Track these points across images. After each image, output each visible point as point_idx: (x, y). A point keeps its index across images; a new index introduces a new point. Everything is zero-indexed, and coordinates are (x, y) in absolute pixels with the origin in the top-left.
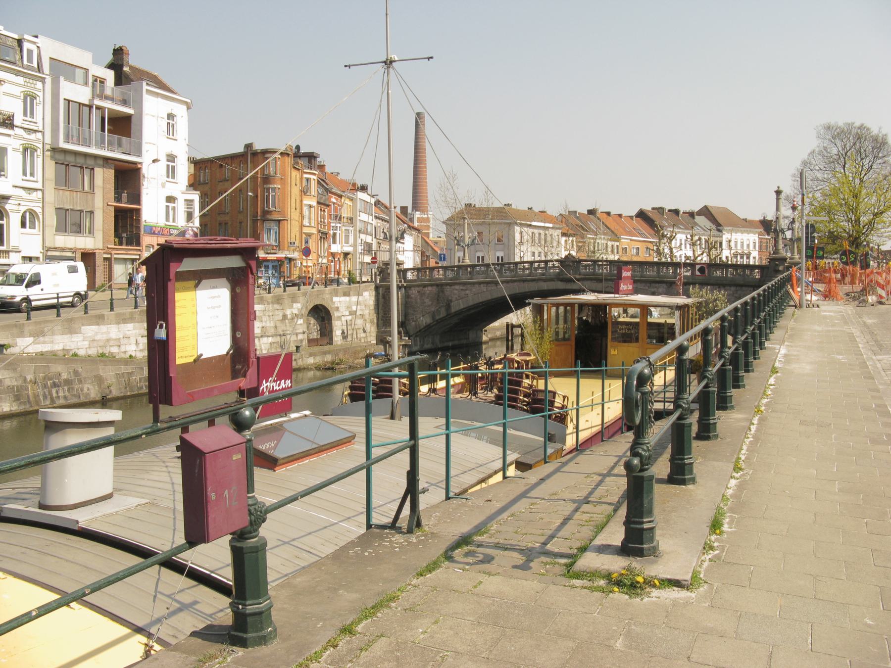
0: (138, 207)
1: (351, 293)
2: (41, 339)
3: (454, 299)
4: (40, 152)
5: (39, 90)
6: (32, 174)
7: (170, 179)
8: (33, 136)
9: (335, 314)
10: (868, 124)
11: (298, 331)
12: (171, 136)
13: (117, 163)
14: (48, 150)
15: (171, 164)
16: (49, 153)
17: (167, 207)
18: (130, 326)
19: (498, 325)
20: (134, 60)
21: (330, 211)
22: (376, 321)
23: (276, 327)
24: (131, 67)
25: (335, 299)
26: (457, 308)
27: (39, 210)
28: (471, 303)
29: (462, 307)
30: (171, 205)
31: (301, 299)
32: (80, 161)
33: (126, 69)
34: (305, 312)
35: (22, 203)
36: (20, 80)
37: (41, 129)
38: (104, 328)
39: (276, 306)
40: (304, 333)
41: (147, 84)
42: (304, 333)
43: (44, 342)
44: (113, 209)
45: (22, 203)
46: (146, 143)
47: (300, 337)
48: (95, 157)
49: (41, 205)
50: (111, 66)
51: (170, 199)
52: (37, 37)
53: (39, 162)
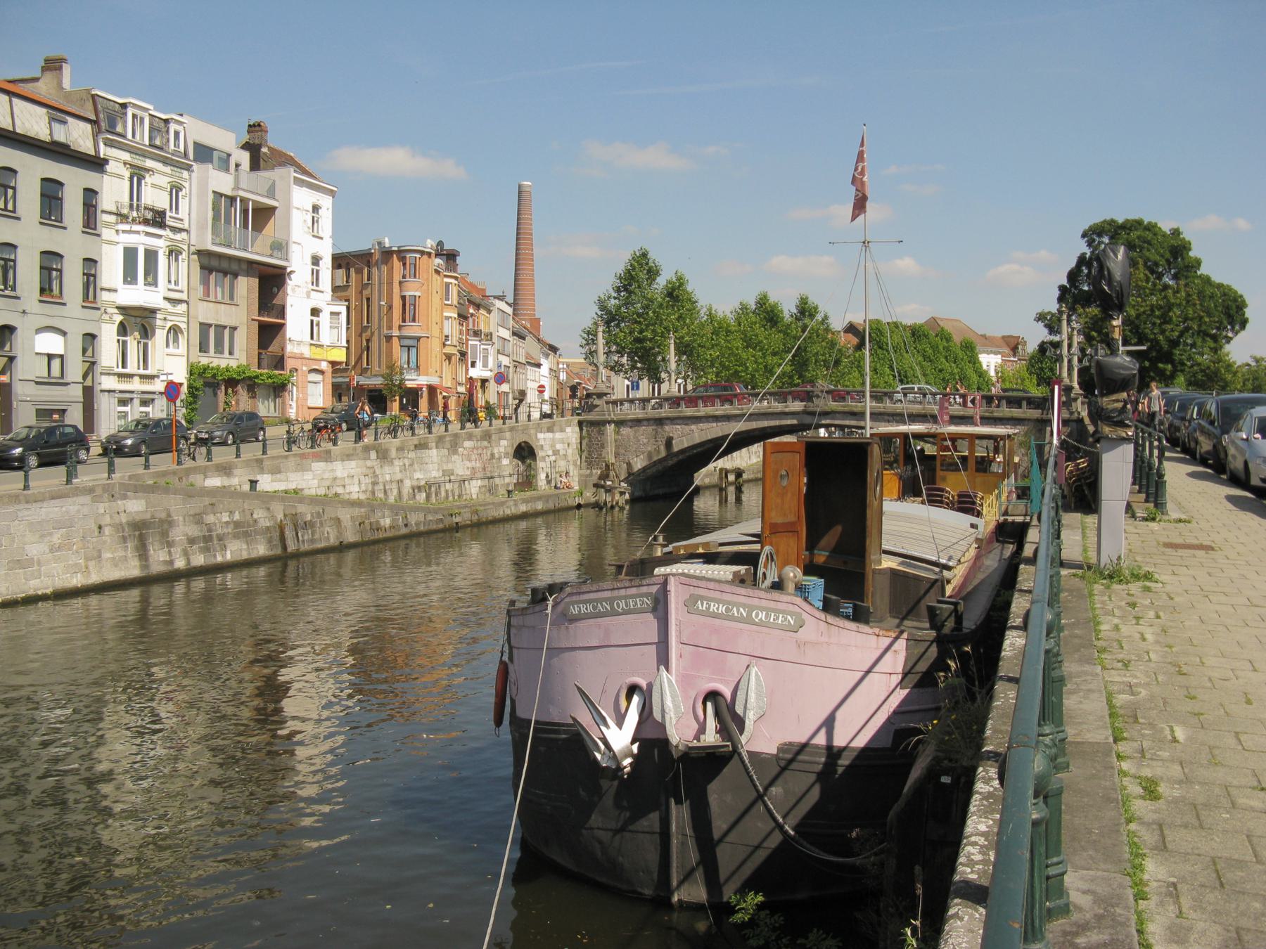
0: (282, 321)
1: (555, 428)
2: (278, 476)
3: (675, 436)
4: (184, 255)
5: (185, 180)
6: (176, 283)
7: (315, 288)
8: (178, 237)
9: (540, 454)
10: (1115, 218)
11: (505, 473)
12: (316, 234)
13: (262, 267)
14: (193, 254)
15: (315, 268)
16: (195, 257)
17: (312, 322)
18: (353, 464)
19: (703, 476)
20: (274, 140)
21: (467, 325)
22: (579, 463)
23: (484, 469)
24: (270, 148)
25: (540, 436)
26: (681, 447)
27: (183, 326)
28: (697, 441)
29: (686, 445)
30: (315, 319)
31: (508, 435)
32: (225, 265)
33: (264, 150)
34: (511, 451)
35: (169, 317)
36: (168, 169)
37: (186, 226)
38: (330, 466)
39: (485, 443)
40: (510, 475)
41: (295, 171)
42: (510, 475)
43: (280, 481)
44: (256, 324)
45: (169, 318)
46: (103, 212)
47: (507, 480)
48: (239, 260)
49: (185, 320)
50: (246, 146)
51: (315, 312)
52: (181, 115)
53: (183, 266)
